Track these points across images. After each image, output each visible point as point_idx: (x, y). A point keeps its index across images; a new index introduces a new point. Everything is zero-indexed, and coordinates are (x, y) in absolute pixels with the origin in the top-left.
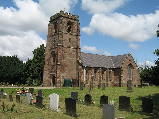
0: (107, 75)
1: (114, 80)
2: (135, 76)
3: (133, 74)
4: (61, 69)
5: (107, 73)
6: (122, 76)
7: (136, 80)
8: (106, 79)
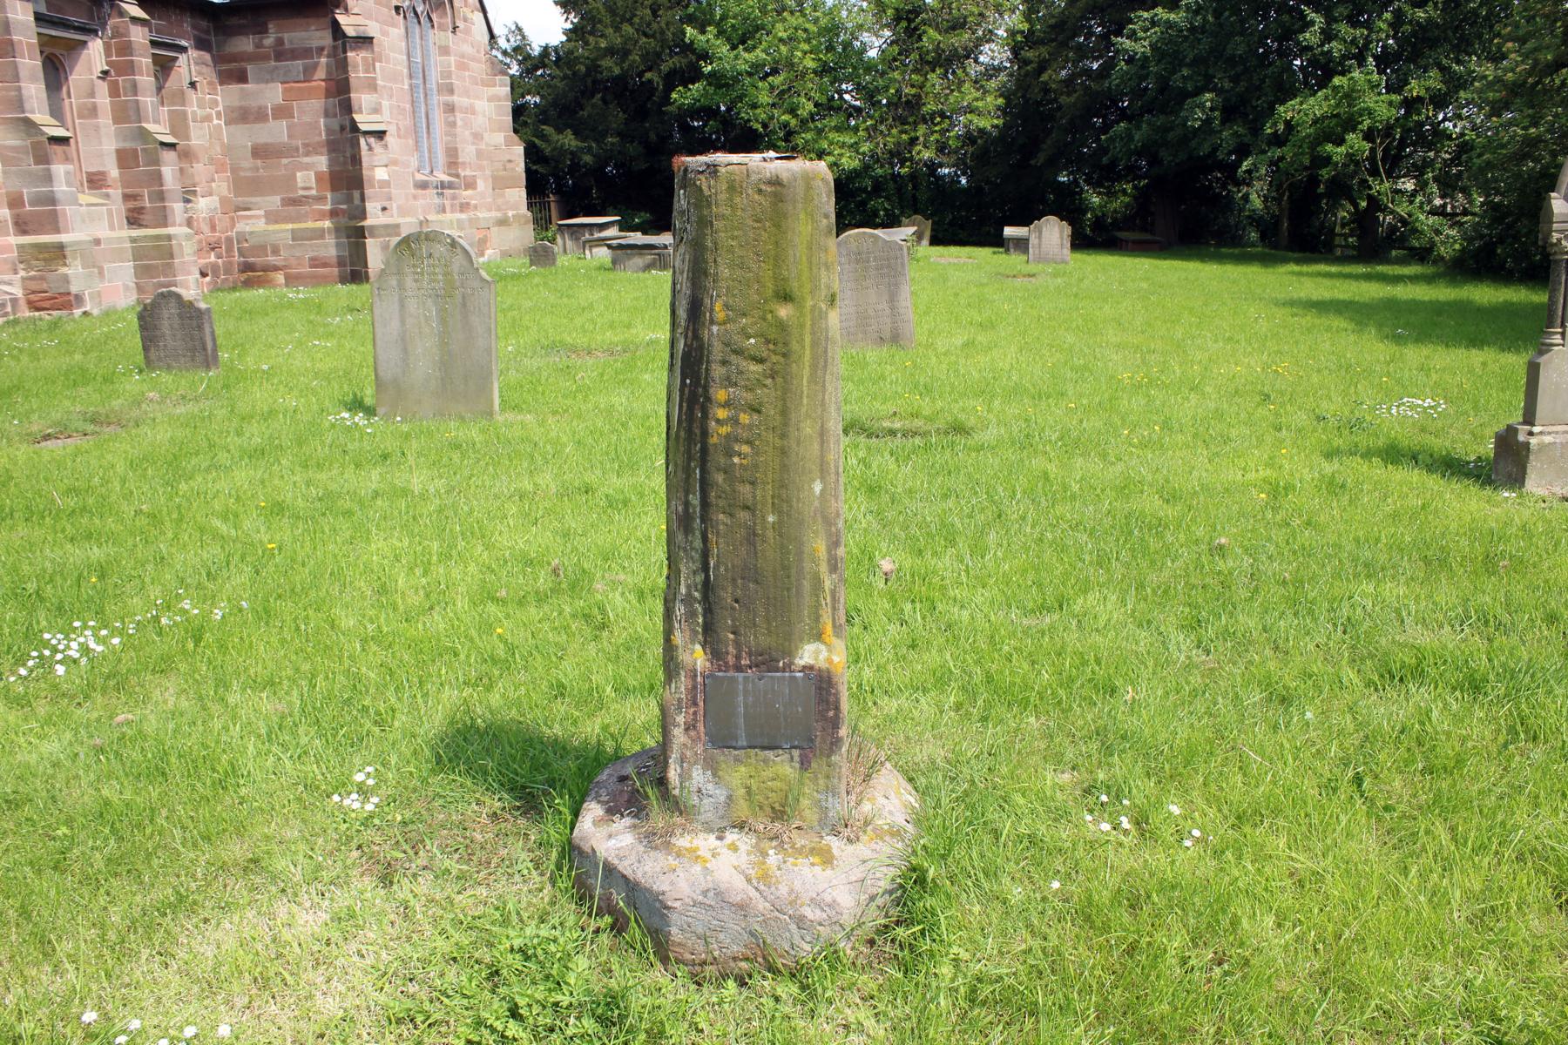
0: (127, 113)
1: (222, 186)
2: (477, 137)
3: (450, 109)
4: (259, 946)
5: (118, 71)
6: (364, 120)
7: (481, 184)
8: (114, 172)
